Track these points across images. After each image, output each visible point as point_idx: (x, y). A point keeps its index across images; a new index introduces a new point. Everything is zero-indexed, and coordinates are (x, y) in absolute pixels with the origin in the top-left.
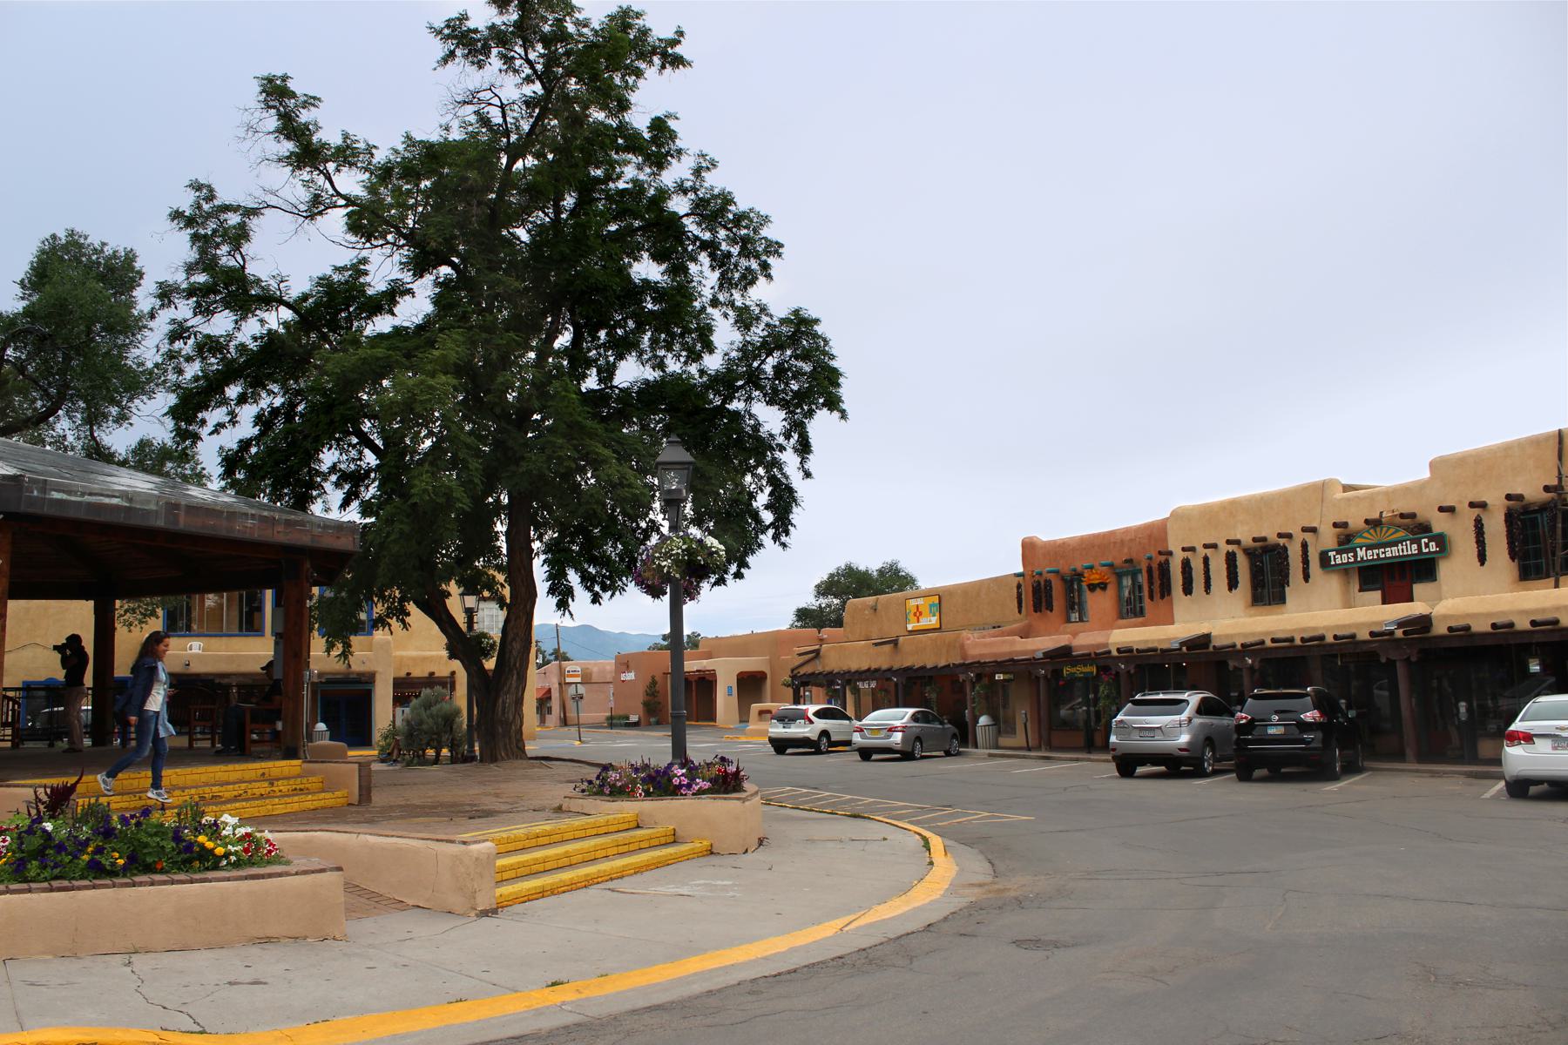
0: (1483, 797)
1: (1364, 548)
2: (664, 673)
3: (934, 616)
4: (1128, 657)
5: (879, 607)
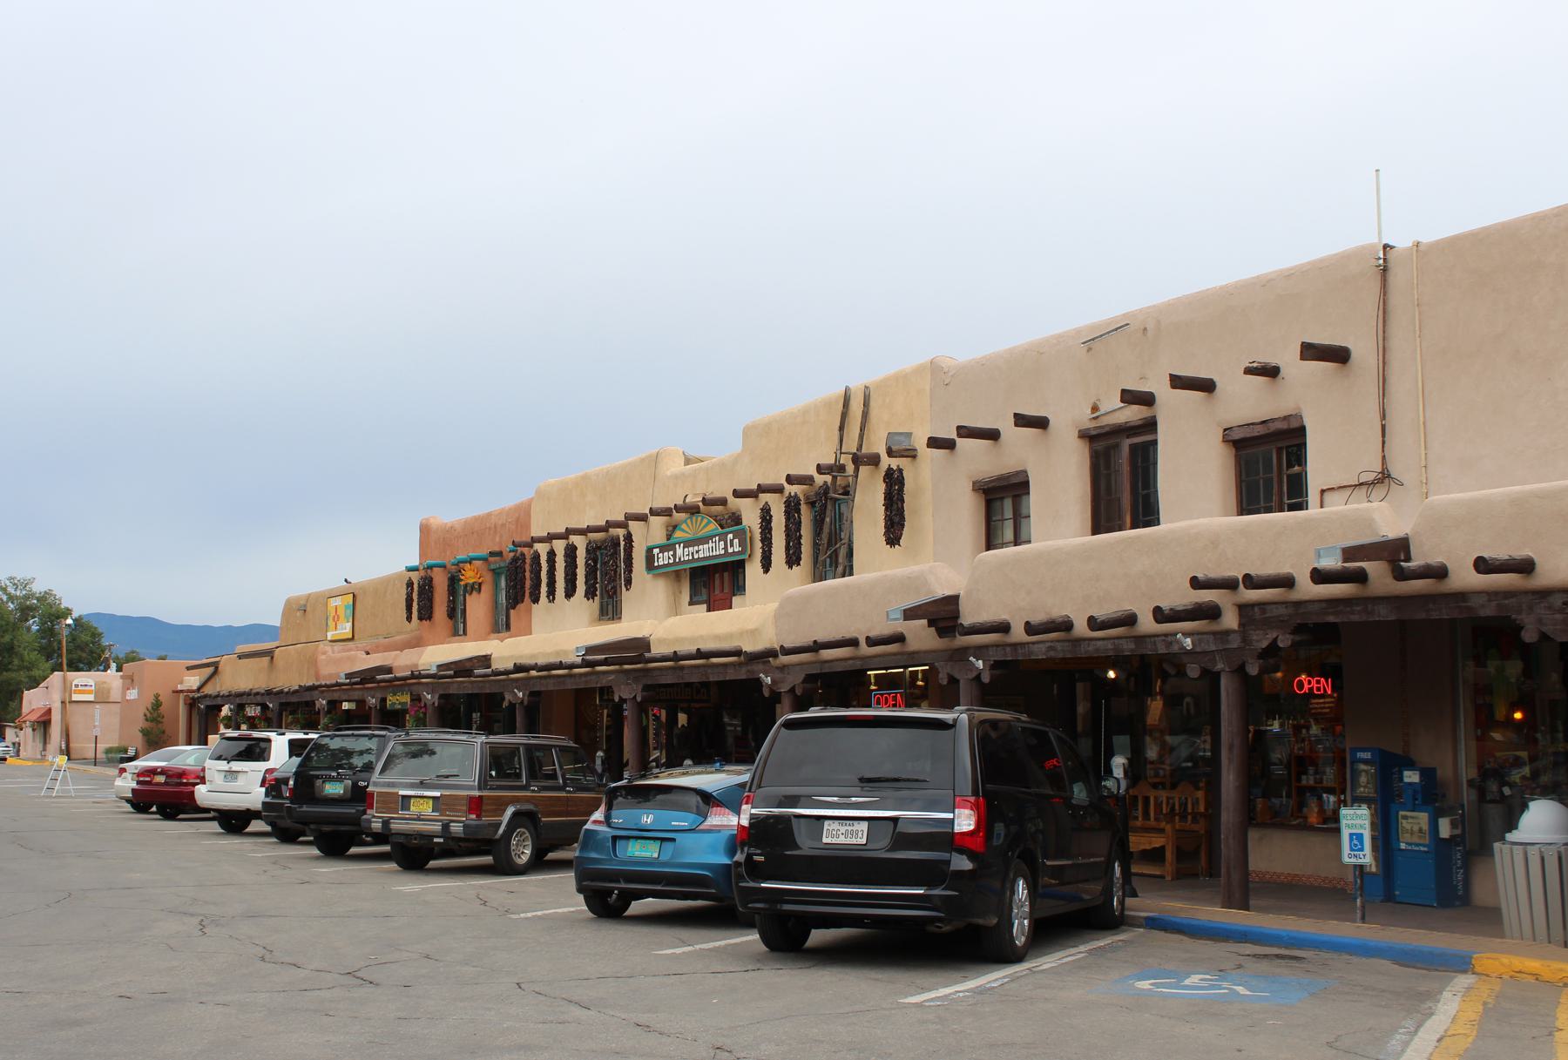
0: (546, 858)
1: (682, 545)
2: (174, 692)
3: (348, 622)
5: (308, 609)
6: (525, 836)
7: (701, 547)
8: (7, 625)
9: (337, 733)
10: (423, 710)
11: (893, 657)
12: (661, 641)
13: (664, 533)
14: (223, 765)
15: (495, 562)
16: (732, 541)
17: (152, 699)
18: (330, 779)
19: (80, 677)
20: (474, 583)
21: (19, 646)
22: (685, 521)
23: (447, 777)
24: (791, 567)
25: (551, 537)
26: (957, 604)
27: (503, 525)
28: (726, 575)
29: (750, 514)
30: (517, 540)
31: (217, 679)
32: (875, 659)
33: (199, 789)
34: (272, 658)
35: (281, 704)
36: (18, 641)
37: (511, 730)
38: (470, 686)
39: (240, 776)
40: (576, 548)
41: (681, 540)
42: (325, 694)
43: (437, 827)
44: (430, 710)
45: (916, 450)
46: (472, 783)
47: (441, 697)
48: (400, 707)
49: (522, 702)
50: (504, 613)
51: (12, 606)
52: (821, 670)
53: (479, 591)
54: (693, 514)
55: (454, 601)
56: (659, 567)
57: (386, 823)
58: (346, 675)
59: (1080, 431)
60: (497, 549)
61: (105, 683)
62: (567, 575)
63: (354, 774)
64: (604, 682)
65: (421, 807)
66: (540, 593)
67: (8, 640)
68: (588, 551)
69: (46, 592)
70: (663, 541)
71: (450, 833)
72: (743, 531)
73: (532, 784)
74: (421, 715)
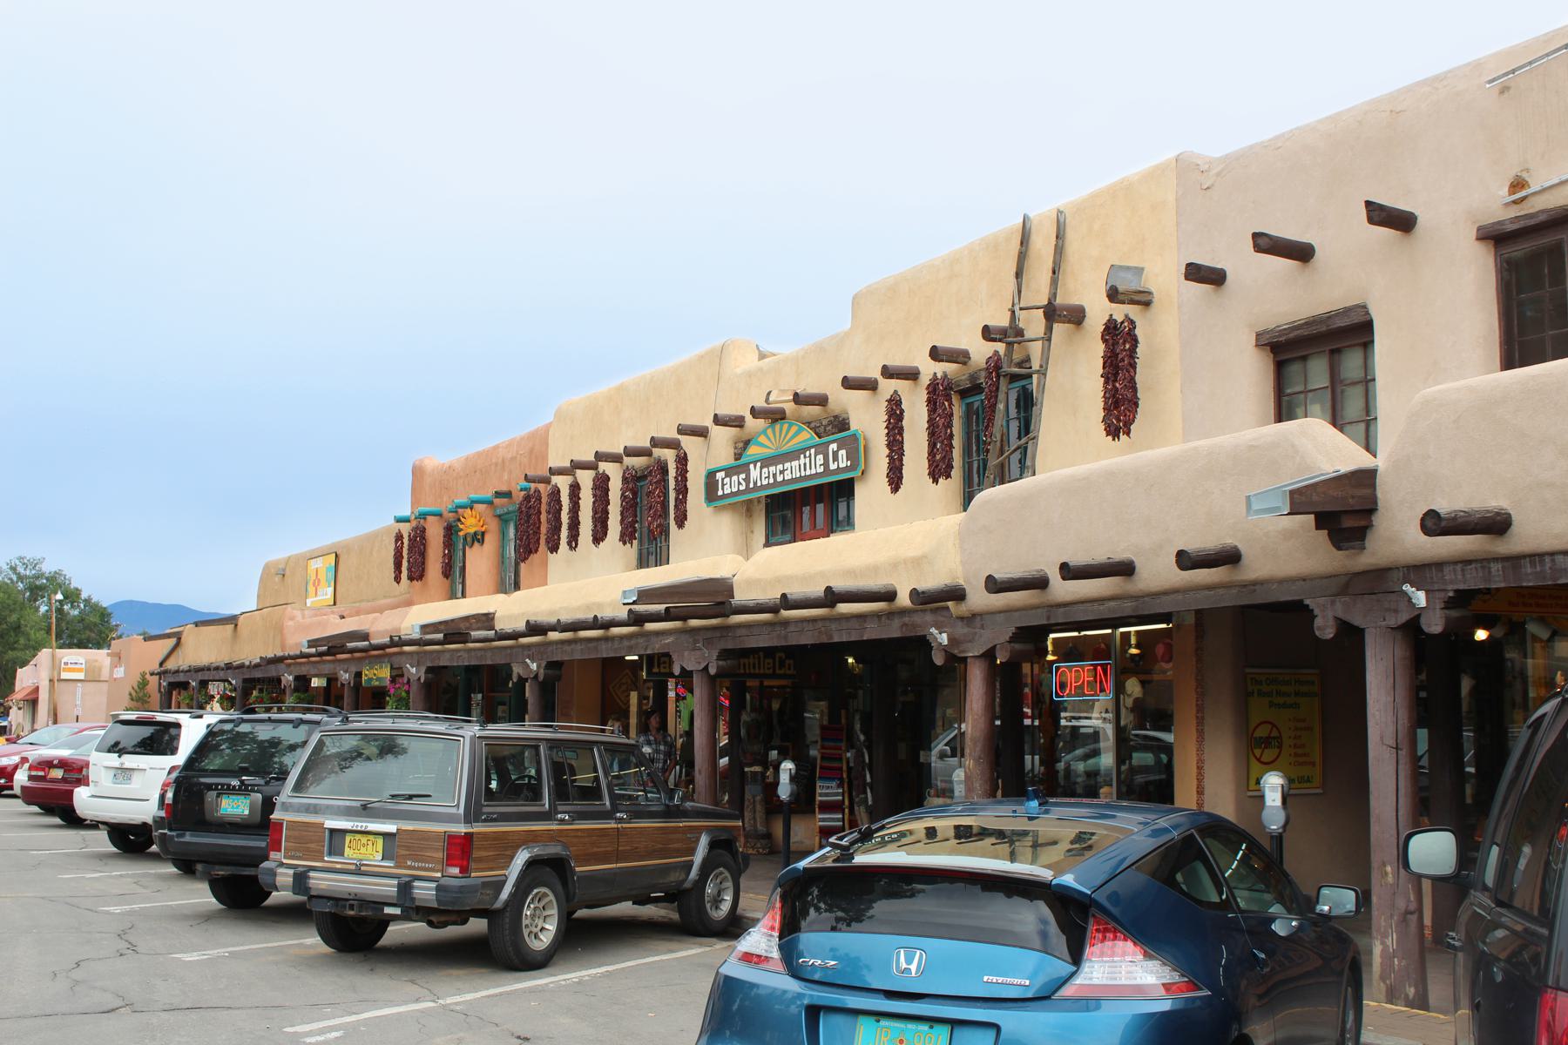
1: (759, 464)
3: (329, 586)
4: (511, 647)
5: (288, 573)
6: (547, 900)
7: (787, 465)
8: (14, 604)
9: (245, 717)
10: (406, 687)
11: (1207, 592)
12: (750, 583)
13: (731, 451)
14: (113, 760)
15: (503, 506)
16: (835, 454)
17: (138, 678)
18: (230, 790)
19: (71, 654)
20: (475, 533)
21: (26, 626)
22: (764, 432)
23: (411, 797)
24: (936, 481)
25: (577, 465)
26: (1373, 486)
27: (513, 459)
28: (820, 507)
29: (867, 418)
30: (531, 473)
31: (179, 651)
32: (1164, 598)
33: (79, 792)
34: (236, 625)
35: (245, 681)
36: (25, 620)
37: (518, 716)
38: (466, 655)
39: (136, 777)
40: (608, 479)
41: (758, 457)
42: (292, 668)
43: (388, 888)
44: (414, 688)
45: (1150, 293)
46: (454, 811)
47: (429, 670)
48: (377, 683)
49: (536, 676)
50: (512, 569)
51: (21, 585)
52: (1048, 618)
53: (482, 542)
54: (775, 421)
55: (450, 558)
56: (725, 496)
57: (300, 880)
58: (309, 641)
59: (1479, 229)
60: (504, 488)
61: (97, 661)
62: (595, 512)
63: (267, 783)
64: (656, 647)
65: (363, 850)
66: (559, 539)
67: (16, 619)
68: (625, 479)
69: (56, 572)
70: (731, 462)
71: (413, 899)
72: (854, 437)
73: (560, 808)
74: (404, 694)
